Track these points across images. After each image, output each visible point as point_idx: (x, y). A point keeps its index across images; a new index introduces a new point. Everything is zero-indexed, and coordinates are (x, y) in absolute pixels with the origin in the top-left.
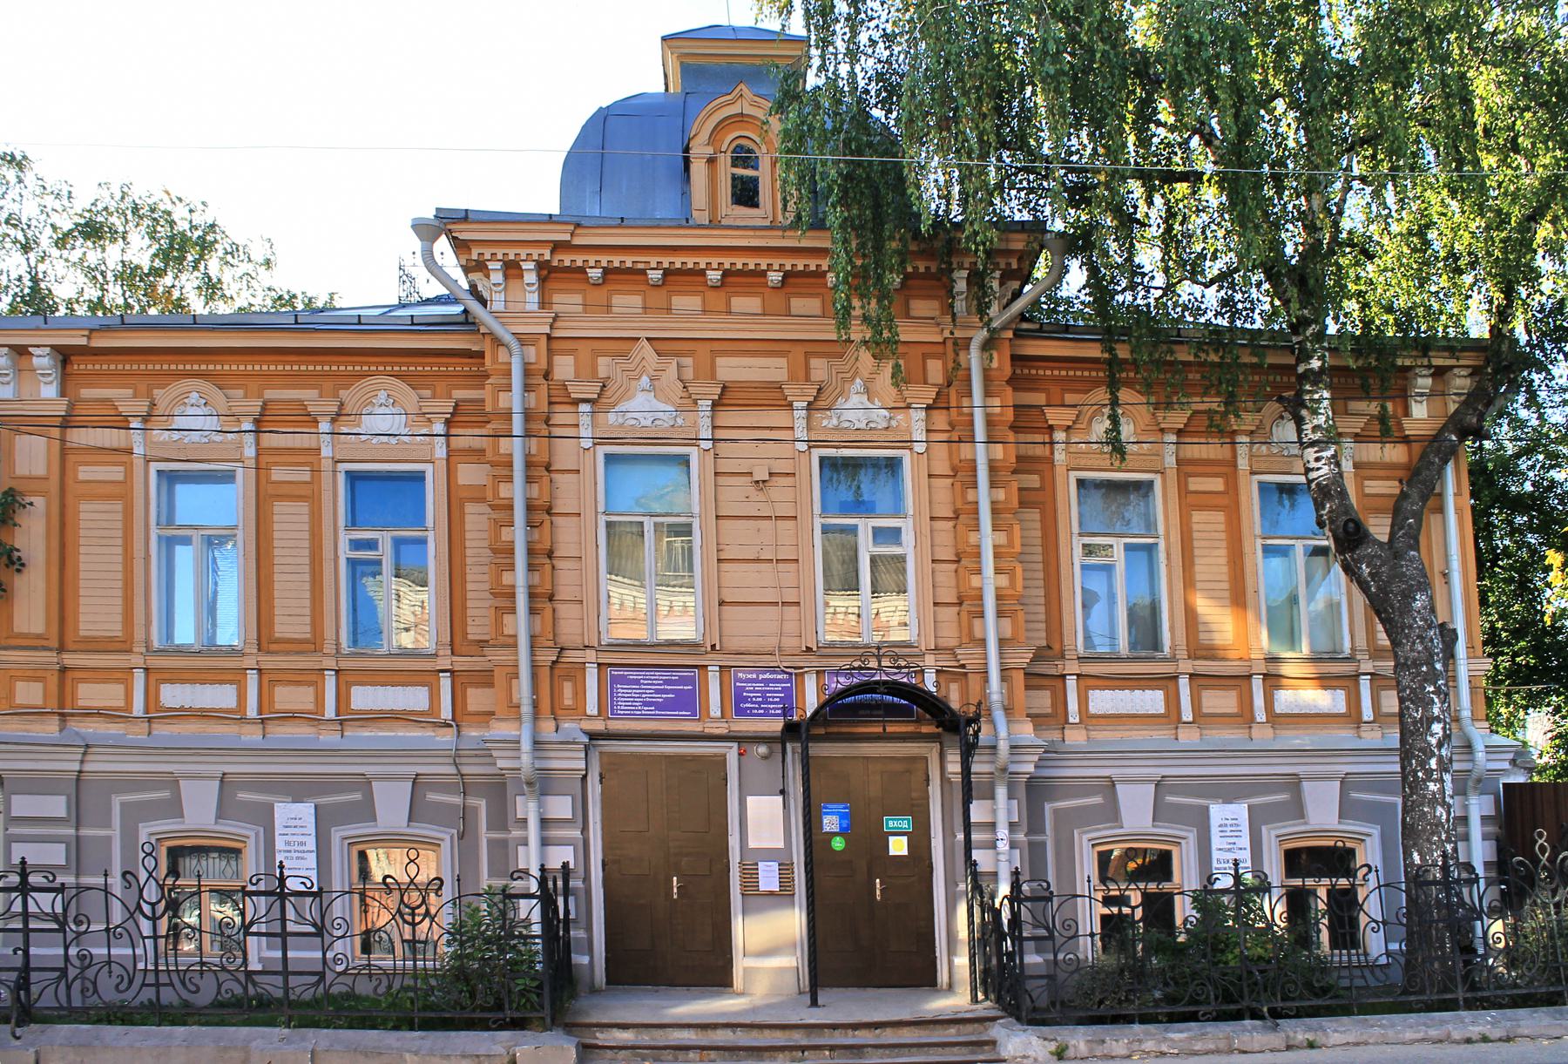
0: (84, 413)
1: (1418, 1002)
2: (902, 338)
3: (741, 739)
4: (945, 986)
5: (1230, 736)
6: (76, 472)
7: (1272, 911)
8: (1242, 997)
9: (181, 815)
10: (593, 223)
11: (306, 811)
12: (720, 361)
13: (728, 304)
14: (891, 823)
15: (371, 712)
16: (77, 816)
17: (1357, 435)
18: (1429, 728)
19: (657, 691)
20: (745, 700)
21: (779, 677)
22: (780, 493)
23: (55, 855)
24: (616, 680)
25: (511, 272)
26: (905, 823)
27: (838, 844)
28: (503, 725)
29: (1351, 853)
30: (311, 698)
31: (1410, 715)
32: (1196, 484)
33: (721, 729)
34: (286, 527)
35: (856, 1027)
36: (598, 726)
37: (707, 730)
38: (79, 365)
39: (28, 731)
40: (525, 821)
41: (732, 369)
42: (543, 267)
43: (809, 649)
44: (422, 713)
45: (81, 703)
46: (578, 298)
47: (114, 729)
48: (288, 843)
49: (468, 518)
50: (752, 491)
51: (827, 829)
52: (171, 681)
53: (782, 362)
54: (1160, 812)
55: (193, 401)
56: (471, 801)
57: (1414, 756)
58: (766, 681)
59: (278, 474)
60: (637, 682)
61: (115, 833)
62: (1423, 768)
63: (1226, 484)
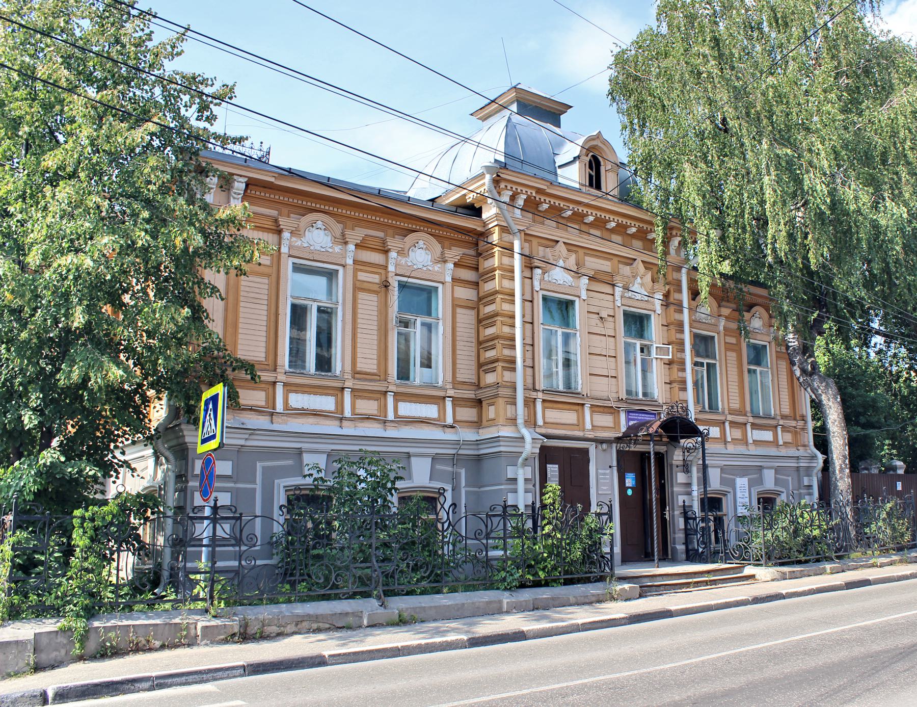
10: (512, 169)
12: (587, 258)
28: (506, 428)
30: (357, 406)
32: (362, 276)
33: (590, 435)
34: (370, 308)
36: (543, 431)
40: (516, 480)
44: (434, 419)
50: (598, 322)
51: (627, 485)
52: (296, 392)
53: (608, 263)
56: (459, 470)
59: (362, 276)
61: (258, 487)
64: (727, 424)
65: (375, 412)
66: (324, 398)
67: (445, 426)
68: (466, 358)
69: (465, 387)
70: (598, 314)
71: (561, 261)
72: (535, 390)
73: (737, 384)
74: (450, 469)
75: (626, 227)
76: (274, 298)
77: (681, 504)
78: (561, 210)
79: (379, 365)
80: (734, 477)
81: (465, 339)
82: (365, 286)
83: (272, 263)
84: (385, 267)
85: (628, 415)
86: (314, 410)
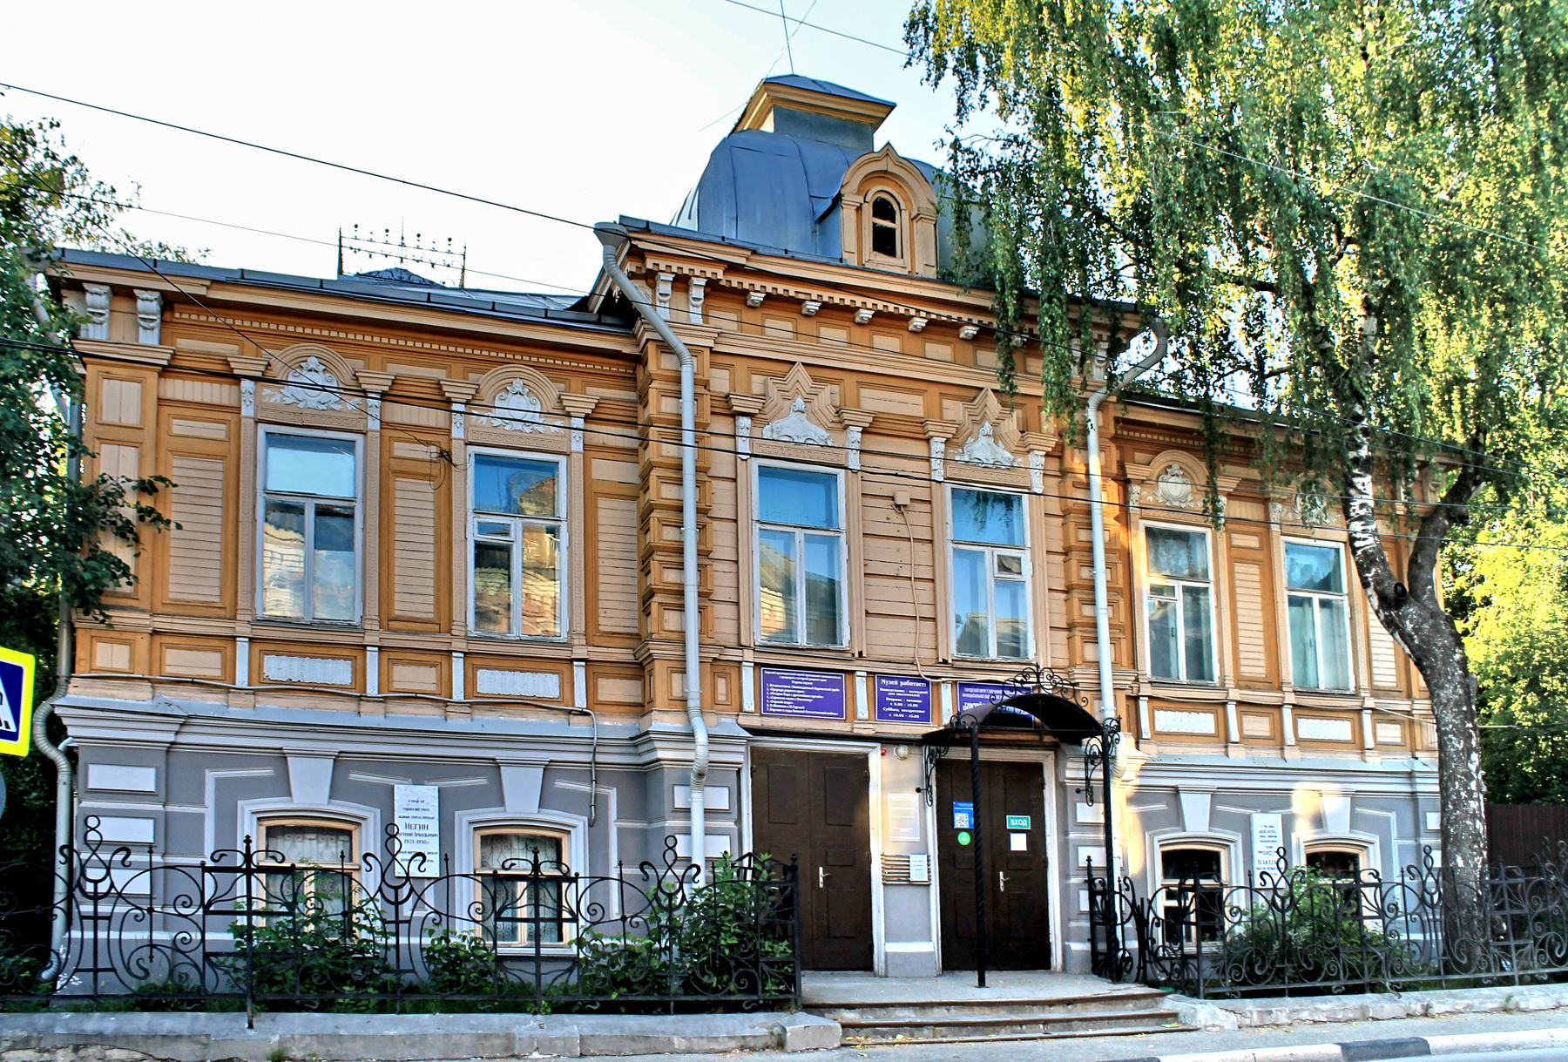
0: (608, 411)
1: (1487, 978)
2: (1021, 390)
3: (888, 742)
4: (1059, 967)
5: (425, 716)
6: (169, 425)
7: (578, 903)
8: (1363, 974)
9: (501, 802)
10: (767, 252)
11: (428, 794)
12: (865, 392)
13: (871, 340)
14: (1013, 821)
15: (499, 696)
16: (165, 792)
17: (587, 415)
18: (1469, 757)
19: (808, 692)
20: (888, 704)
21: (918, 684)
22: (918, 519)
23: (142, 831)
24: (768, 679)
25: (679, 285)
26: (1024, 822)
27: (964, 839)
28: (665, 717)
29: (1354, 858)
30: (1245, 726)
31: (1453, 746)
32: (401, 449)
35: (1051, 1003)
36: (756, 722)
37: (855, 731)
38: (182, 315)
39: (113, 696)
40: (688, 811)
41: (876, 401)
42: (713, 287)
43: (945, 662)
45: (396, 686)
46: (789, 326)
47: (210, 702)
48: (409, 826)
49: (601, 512)
51: (957, 825)
52: (277, 653)
53: (919, 399)
54: (1215, 818)
55: (311, 366)
56: (603, 791)
57: (1456, 779)
58: (907, 689)
59: (401, 449)
60: (788, 682)
62: (1465, 789)
63: (1261, 542)
64: (1231, 708)
65: (433, 688)
66: (331, 664)
67: (570, 712)
68: (618, 588)
69: (618, 642)
70: (893, 498)
71: (987, 424)
72: (741, 646)
73: (1261, 628)
74: (586, 788)
75: (956, 326)
76: (232, 494)
77: (1083, 863)
78: (853, 310)
79: (437, 604)
80: (1247, 811)
81: (618, 555)
82: (410, 466)
83: (228, 436)
84: (237, 410)
85: (962, 691)
86: (310, 684)
